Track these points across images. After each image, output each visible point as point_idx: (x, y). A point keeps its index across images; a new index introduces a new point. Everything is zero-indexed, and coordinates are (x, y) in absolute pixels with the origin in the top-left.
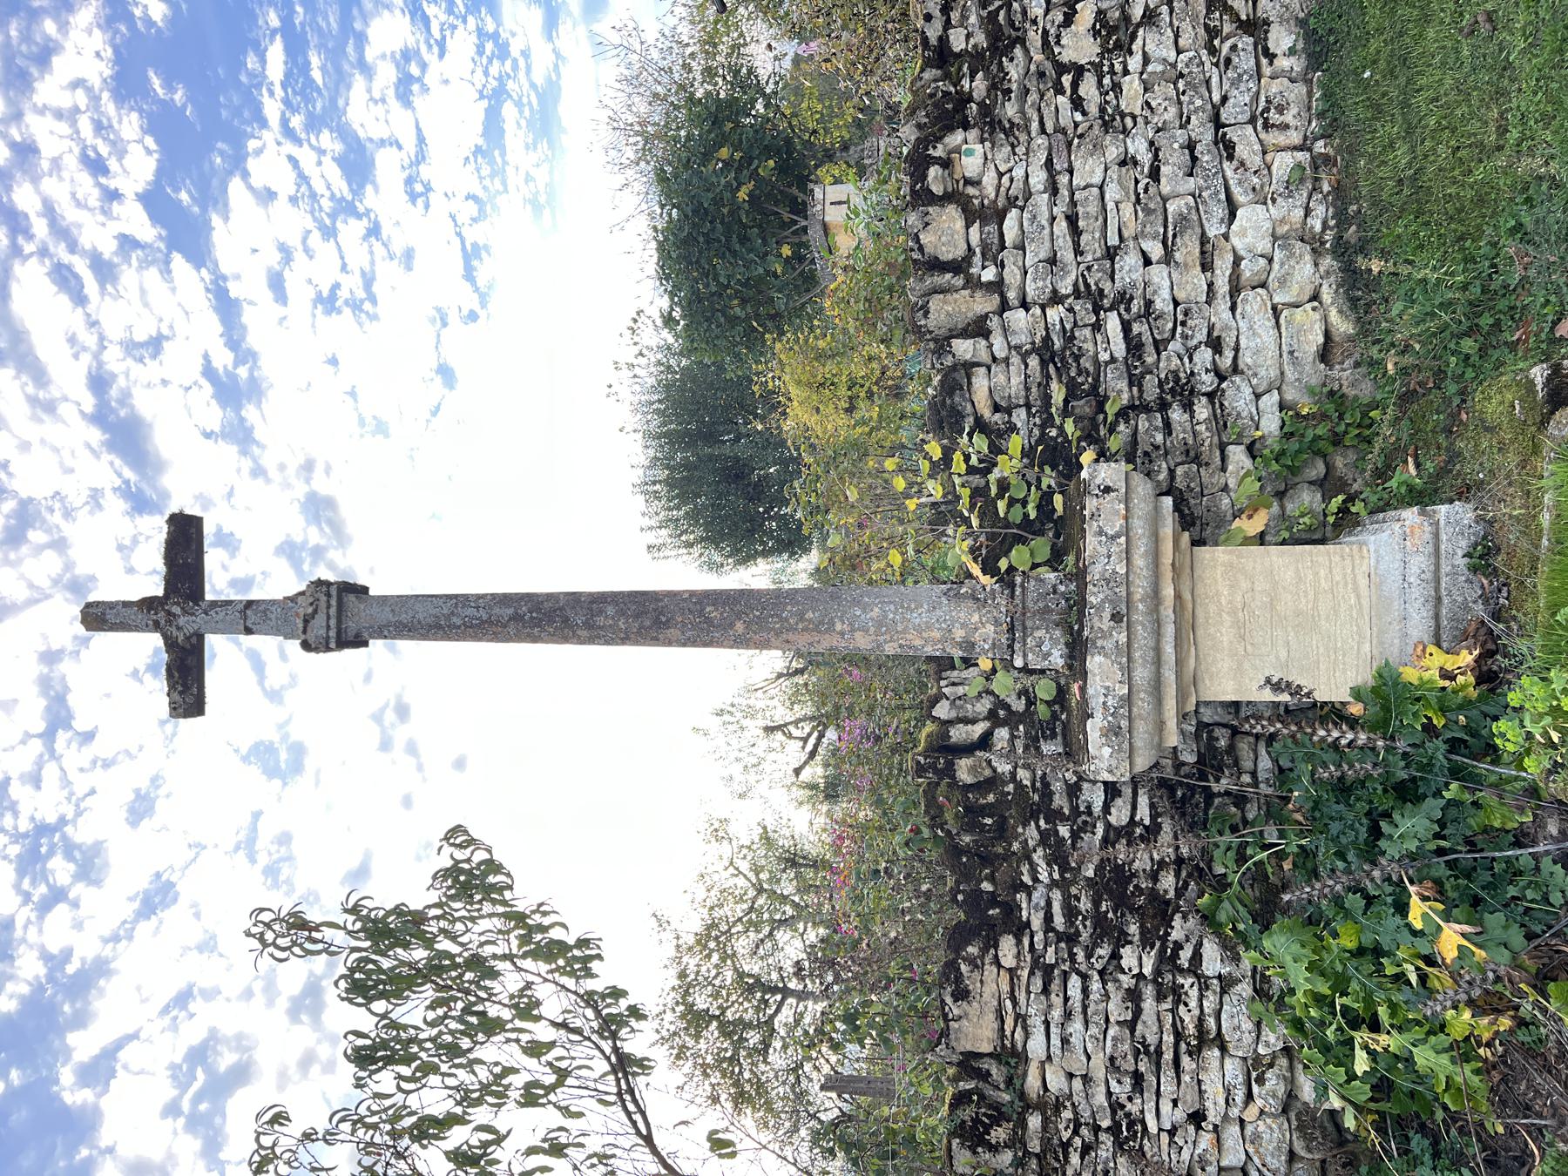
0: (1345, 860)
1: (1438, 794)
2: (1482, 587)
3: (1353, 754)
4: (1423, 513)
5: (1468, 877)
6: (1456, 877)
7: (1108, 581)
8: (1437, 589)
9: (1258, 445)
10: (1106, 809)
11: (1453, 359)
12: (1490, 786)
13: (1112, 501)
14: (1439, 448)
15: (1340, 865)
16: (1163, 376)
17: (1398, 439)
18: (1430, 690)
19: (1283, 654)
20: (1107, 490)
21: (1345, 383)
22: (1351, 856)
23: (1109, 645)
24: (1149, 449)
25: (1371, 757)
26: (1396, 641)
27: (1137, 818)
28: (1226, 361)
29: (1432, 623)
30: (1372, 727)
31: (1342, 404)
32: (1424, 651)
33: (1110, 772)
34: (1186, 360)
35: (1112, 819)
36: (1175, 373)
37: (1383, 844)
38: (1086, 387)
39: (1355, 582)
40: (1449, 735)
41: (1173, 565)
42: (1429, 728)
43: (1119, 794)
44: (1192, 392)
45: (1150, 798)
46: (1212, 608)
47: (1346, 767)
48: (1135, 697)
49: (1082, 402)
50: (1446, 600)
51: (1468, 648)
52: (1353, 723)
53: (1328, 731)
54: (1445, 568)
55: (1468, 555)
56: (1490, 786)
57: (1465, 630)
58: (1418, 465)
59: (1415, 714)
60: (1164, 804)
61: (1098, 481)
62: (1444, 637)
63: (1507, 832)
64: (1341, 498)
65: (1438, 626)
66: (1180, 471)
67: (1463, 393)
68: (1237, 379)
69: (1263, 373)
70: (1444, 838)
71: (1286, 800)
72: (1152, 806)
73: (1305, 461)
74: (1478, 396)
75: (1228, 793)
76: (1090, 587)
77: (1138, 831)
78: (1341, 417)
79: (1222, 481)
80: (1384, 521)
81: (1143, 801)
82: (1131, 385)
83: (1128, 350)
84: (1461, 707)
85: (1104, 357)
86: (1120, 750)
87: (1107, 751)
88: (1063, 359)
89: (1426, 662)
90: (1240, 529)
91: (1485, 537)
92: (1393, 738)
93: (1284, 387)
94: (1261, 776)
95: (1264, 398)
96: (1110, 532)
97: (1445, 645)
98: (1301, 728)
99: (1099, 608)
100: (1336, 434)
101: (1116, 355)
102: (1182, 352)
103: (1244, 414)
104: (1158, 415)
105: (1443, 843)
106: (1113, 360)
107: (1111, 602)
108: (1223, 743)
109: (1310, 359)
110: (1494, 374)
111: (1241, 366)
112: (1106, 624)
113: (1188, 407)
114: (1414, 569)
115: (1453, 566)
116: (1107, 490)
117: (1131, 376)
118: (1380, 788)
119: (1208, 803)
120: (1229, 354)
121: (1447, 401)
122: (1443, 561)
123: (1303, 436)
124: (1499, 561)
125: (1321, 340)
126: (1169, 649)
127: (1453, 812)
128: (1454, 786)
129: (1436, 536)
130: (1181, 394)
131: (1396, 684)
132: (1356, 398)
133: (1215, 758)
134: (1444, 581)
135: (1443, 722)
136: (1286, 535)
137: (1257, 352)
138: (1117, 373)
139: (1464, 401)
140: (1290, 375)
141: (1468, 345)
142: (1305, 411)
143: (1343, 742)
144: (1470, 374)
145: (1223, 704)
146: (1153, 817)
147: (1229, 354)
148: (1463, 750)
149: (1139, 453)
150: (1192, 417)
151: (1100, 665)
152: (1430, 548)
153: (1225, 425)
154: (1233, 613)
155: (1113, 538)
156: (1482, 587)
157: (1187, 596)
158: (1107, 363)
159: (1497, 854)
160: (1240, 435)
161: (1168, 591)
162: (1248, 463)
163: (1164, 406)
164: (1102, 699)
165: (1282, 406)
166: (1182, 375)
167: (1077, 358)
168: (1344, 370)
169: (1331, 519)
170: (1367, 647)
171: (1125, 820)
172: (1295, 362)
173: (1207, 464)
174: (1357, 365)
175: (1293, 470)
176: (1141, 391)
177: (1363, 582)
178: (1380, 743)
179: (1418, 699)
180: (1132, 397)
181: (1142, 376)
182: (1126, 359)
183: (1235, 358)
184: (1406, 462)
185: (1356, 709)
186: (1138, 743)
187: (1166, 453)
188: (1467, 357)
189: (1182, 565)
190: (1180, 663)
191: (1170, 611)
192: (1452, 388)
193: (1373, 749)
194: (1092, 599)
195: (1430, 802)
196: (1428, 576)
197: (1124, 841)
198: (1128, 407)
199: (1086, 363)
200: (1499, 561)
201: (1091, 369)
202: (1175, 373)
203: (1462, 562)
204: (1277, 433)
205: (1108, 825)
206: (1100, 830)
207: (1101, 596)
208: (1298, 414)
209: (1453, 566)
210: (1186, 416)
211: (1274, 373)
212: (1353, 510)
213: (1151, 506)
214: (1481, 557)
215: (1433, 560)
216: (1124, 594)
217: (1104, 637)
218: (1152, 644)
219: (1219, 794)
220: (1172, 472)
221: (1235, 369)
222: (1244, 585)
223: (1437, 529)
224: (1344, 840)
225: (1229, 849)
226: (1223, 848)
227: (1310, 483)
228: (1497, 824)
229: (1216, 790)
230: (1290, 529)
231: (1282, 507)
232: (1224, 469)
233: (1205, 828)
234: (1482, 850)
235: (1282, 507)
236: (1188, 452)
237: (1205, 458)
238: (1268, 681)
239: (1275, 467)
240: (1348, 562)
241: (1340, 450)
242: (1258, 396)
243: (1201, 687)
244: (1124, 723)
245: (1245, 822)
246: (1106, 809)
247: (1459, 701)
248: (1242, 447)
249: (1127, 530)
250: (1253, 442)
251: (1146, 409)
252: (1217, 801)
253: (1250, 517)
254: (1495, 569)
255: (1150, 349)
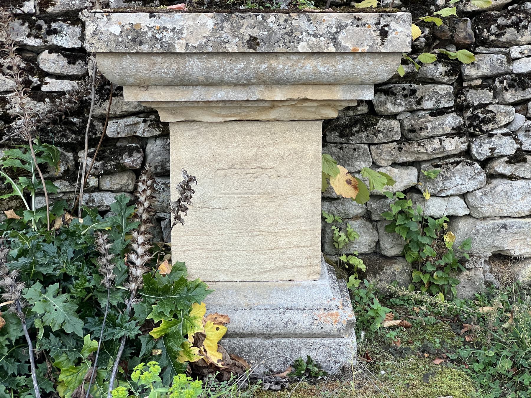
0: (19, 256)
1: (87, 331)
2: (280, 372)
3: (121, 264)
4: (349, 324)
5: (11, 356)
6: (9, 346)
7: (290, 34)
8: (278, 335)
9: (416, 196)
10: (55, 49)
11: (492, 353)
12: (97, 372)
13: (372, 39)
14: (408, 343)
15: (15, 252)
16: (491, 108)
17: (417, 314)
18: (185, 326)
19: (215, 203)
20: (384, 34)
21: (472, 273)
22: (23, 260)
23: (225, 34)
24: (418, 95)
25: (119, 279)
26: (229, 302)
27: (47, 79)
28: (500, 167)
29: (246, 331)
30: (148, 279)
31: (453, 270)
32: (221, 323)
33: (95, 33)
34: (505, 130)
35: (45, 55)
36: (493, 120)
37: (38, 286)
38: (485, 34)
39: (285, 268)
40: (143, 340)
41: (305, 100)
42: (148, 325)
43: (72, 61)
44: (472, 135)
45: (69, 92)
46: (261, 139)
47: (109, 257)
48: (172, 59)
49: (470, 31)
50: (268, 342)
51: (224, 359)
52: (152, 264)
53: (143, 244)
54: (297, 342)
55: (310, 360)
56: (97, 373)
57: (240, 358)
58: (393, 328)
59: (162, 314)
60: (64, 104)
61: (393, 25)
62: (234, 340)
63: (55, 387)
64: (363, 267)
65: (243, 336)
66: (395, 124)
67: (460, 361)
68: (482, 177)
69: (487, 200)
70: (46, 335)
71: (75, 213)
72: (61, 94)
73: (400, 236)
74: (456, 372)
75: (78, 165)
76: (284, 16)
77: (35, 80)
78: (440, 268)
79: (383, 163)
80: (342, 296)
81: (65, 85)
82: (485, 78)
83: (519, 75)
84: (169, 350)
85: (515, 52)
86: (118, 43)
87: (116, 30)
88: (514, 10)
89: (211, 325)
90: (337, 173)
91: (325, 374)
92: (138, 296)
93: (471, 220)
94: (96, 196)
95: (462, 202)
96: (340, 37)
97: (226, 341)
98: (145, 222)
99: (262, 25)
100: (424, 264)
101: (516, 64)
102: (513, 127)
103: (447, 184)
104: (451, 104)
105: (41, 335)
106: (511, 60)
107: (269, 37)
108: (127, 160)
109: (497, 244)
110: (477, 385)
111: (495, 182)
112: (247, 31)
113: (458, 132)
114: (296, 316)
115: (299, 349)
116: (384, 34)
117: (492, 78)
118: (91, 285)
119: (69, 147)
120: (507, 170)
121: (454, 349)
122: (304, 340)
123: (424, 234)
124: (304, 383)
125: (516, 253)
126: (221, 94)
127: (71, 343)
128: (96, 344)
129: (328, 335)
130: (470, 126)
131: (189, 299)
132: (457, 282)
133: (112, 153)
134: (287, 341)
135: (155, 336)
136: (329, 220)
137: (507, 195)
138: (497, 65)
139: (452, 361)
140: (482, 226)
141: (505, 365)
142: (447, 238)
143: (133, 257)
144: (477, 367)
145: (167, 160)
146: (50, 94)
147: (507, 170)
148: (128, 354)
149: (415, 86)
150: (447, 135)
151: (204, 25)
152: (316, 330)
153: (437, 166)
154: (257, 158)
155: (334, 39)
156: (280, 372)
157: (273, 114)
158: (508, 54)
159: (33, 375)
160: (428, 179)
161: (279, 94)
162: (400, 186)
163: (460, 109)
164: (169, 26)
165: (452, 218)
166: (490, 126)
167: (516, 25)
168: (484, 272)
169: (343, 258)
170: (223, 277)
171: (45, 66)
172: (496, 230)
173: (400, 149)
174: (488, 284)
175: (391, 227)
176: (477, 87)
177: (286, 275)
178: (133, 286)
179: (175, 316)
180: (471, 80)
181: (492, 88)
182: (511, 73)
183: (503, 176)
184: (395, 319)
185: (164, 268)
186: (126, 62)
187: (413, 112)
188: (494, 365)
189: (303, 109)
190: (207, 104)
191: (260, 97)
192: (465, 353)
193: (127, 280)
194: (272, 18)
195: (80, 324)
196: (291, 328)
197: (23, 65)
198: (461, 75)
199: (510, 34)
200: (304, 383)
201: (503, 39)
202: (493, 120)
203: (304, 355)
204: (427, 213)
205: (38, 51)
206: (32, 42)
207: (275, 27)
208: (444, 232)
209: (299, 349)
210: (449, 130)
211: (486, 211)
212: (352, 278)
213: (365, 78)
214: (308, 370)
215: (306, 332)
216: (277, 50)
217: (233, 29)
218: (227, 77)
219: (76, 158)
220: (394, 116)
221: (492, 176)
222: (284, 169)
223: (334, 336)
224: (39, 254)
225: (23, 162)
226: (24, 157)
227: (378, 243)
228: (62, 377)
229: (80, 154)
230: (335, 222)
231: (356, 218)
232: (394, 164)
233: (41, 142)
234: (36, 367)
235: (356, 218)
236: (413, 131)
237: (407, 147)
238: (192, 179)
239: (395, 210)
240: (305, 262)
241: (408, 268)
242: (464, 196)
243: (183, 127)
244: (145, 48)
245: (51, 180)
246: (55, 49)
247: (175, 348)
248: (414, 181)
249: (342, 54)
250: (419, 192)
251: (459, 92)
252: (70, 155)
253: (349, 182)
254: (296, 381)
255: (520, 95)
